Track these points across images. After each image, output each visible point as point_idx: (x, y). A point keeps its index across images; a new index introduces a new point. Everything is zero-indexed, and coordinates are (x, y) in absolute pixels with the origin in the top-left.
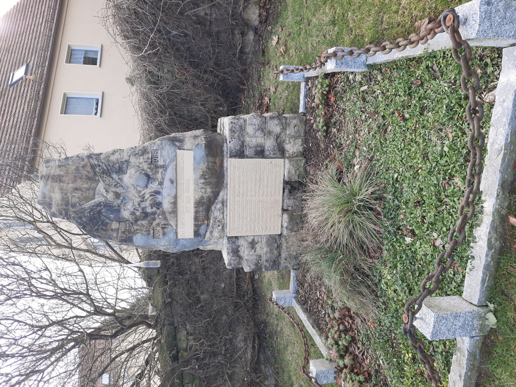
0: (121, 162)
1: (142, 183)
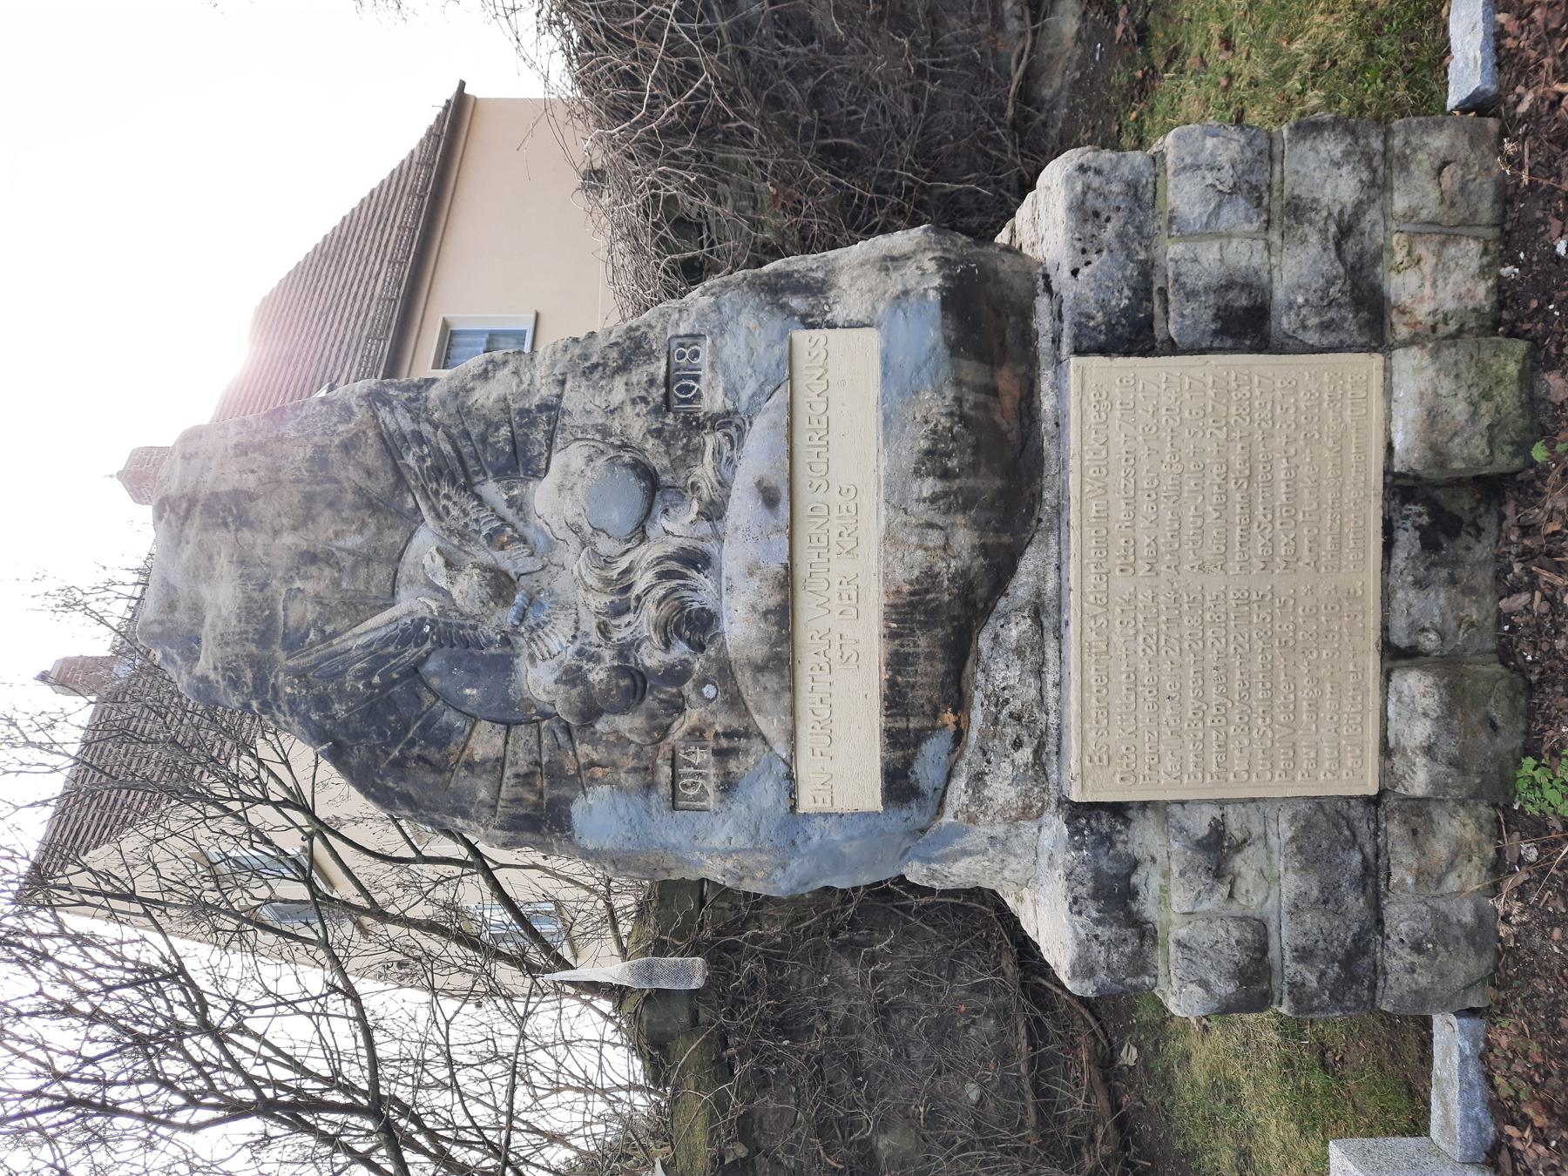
0: (524, 412)
1: (620, 515)
